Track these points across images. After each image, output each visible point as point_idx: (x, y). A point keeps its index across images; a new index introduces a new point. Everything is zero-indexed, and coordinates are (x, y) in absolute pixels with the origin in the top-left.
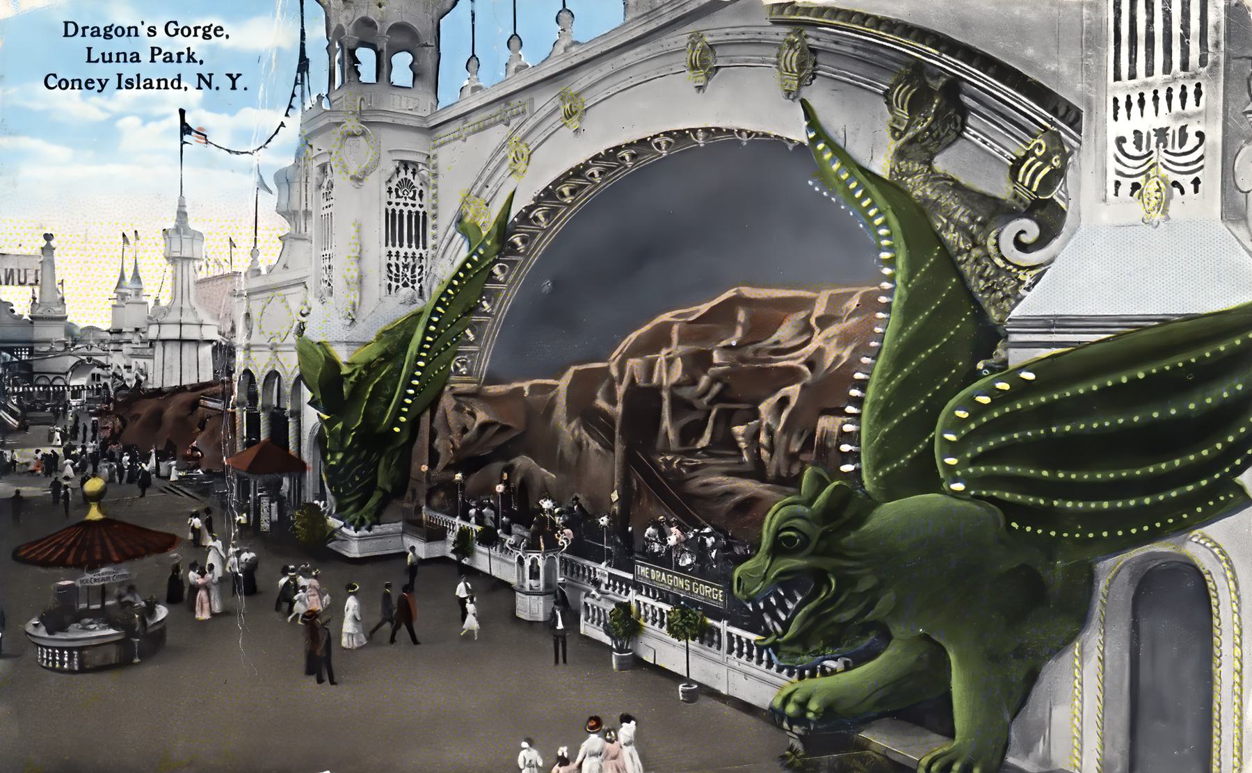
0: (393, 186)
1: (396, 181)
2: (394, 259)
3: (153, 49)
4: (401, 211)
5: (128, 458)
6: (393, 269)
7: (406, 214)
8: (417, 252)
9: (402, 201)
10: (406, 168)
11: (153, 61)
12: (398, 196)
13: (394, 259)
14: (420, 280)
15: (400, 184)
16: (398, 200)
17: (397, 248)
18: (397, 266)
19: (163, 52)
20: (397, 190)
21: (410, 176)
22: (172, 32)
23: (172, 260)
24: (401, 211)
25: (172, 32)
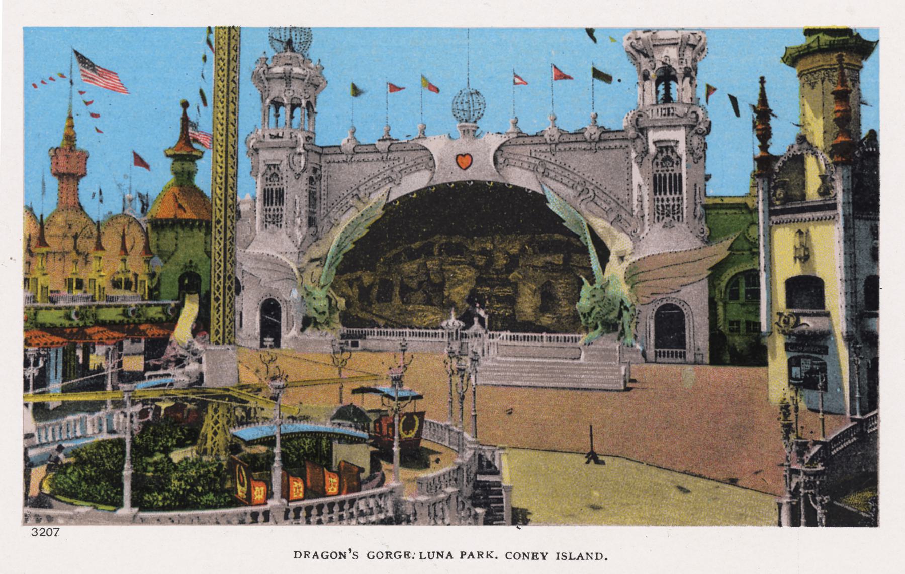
0: (659, 161)
1: (660, 157)
2: (660, 203)
3: (462, 552)
4: (665, 175)
5: (200, 490)
6: (660, 208)
7: (668, 176)
8: (676, 197)
9: (665, 169)
10: (667, 150)
11: (462, 558)
12: (662, 166)
13: (660, 203)
14: (678, 213)
15: (664, 160)
16: (663, 169)
17: (270, 207)
18: (662, 206)
19: (375, 557)
20: (661, 163)
21: (670, 154)
22: (325, 557)
23: (60, 175)
24: (665, 175)
25: (325, 557)
